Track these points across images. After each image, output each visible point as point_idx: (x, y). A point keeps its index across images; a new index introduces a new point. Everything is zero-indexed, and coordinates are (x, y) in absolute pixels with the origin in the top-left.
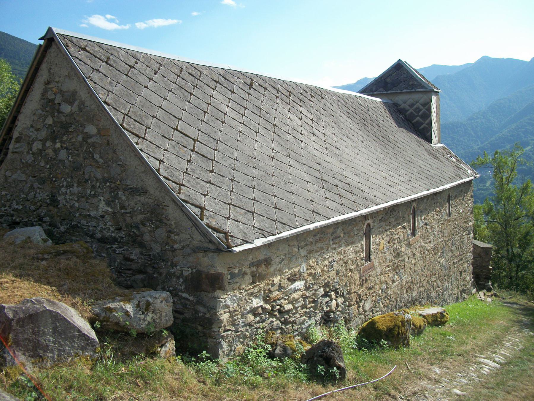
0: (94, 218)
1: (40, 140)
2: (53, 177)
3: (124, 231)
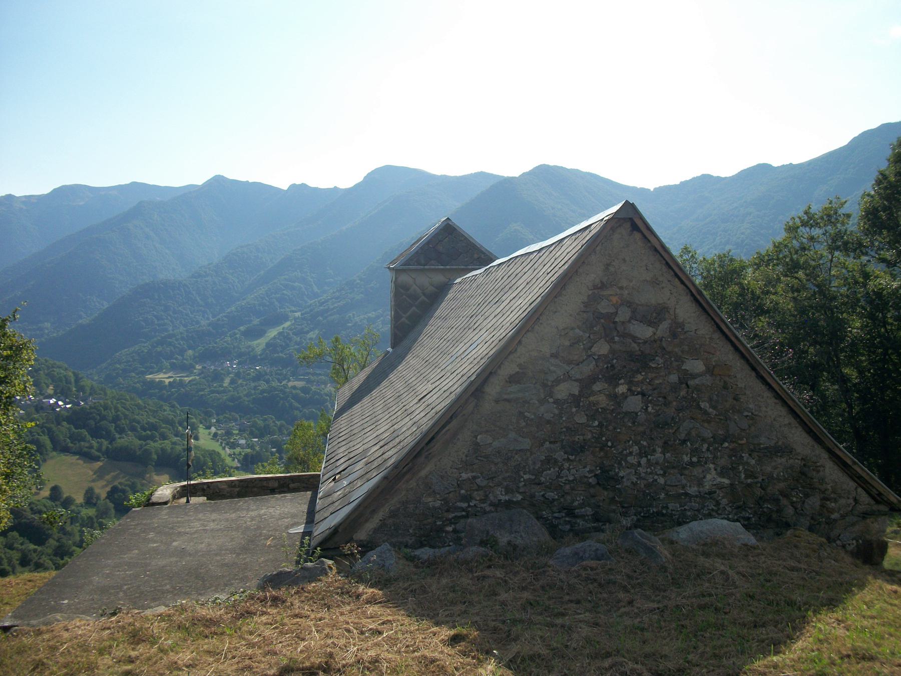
0: (696, 496)
1: (576, 380)
2: (607, 441)
3: (751, 508)
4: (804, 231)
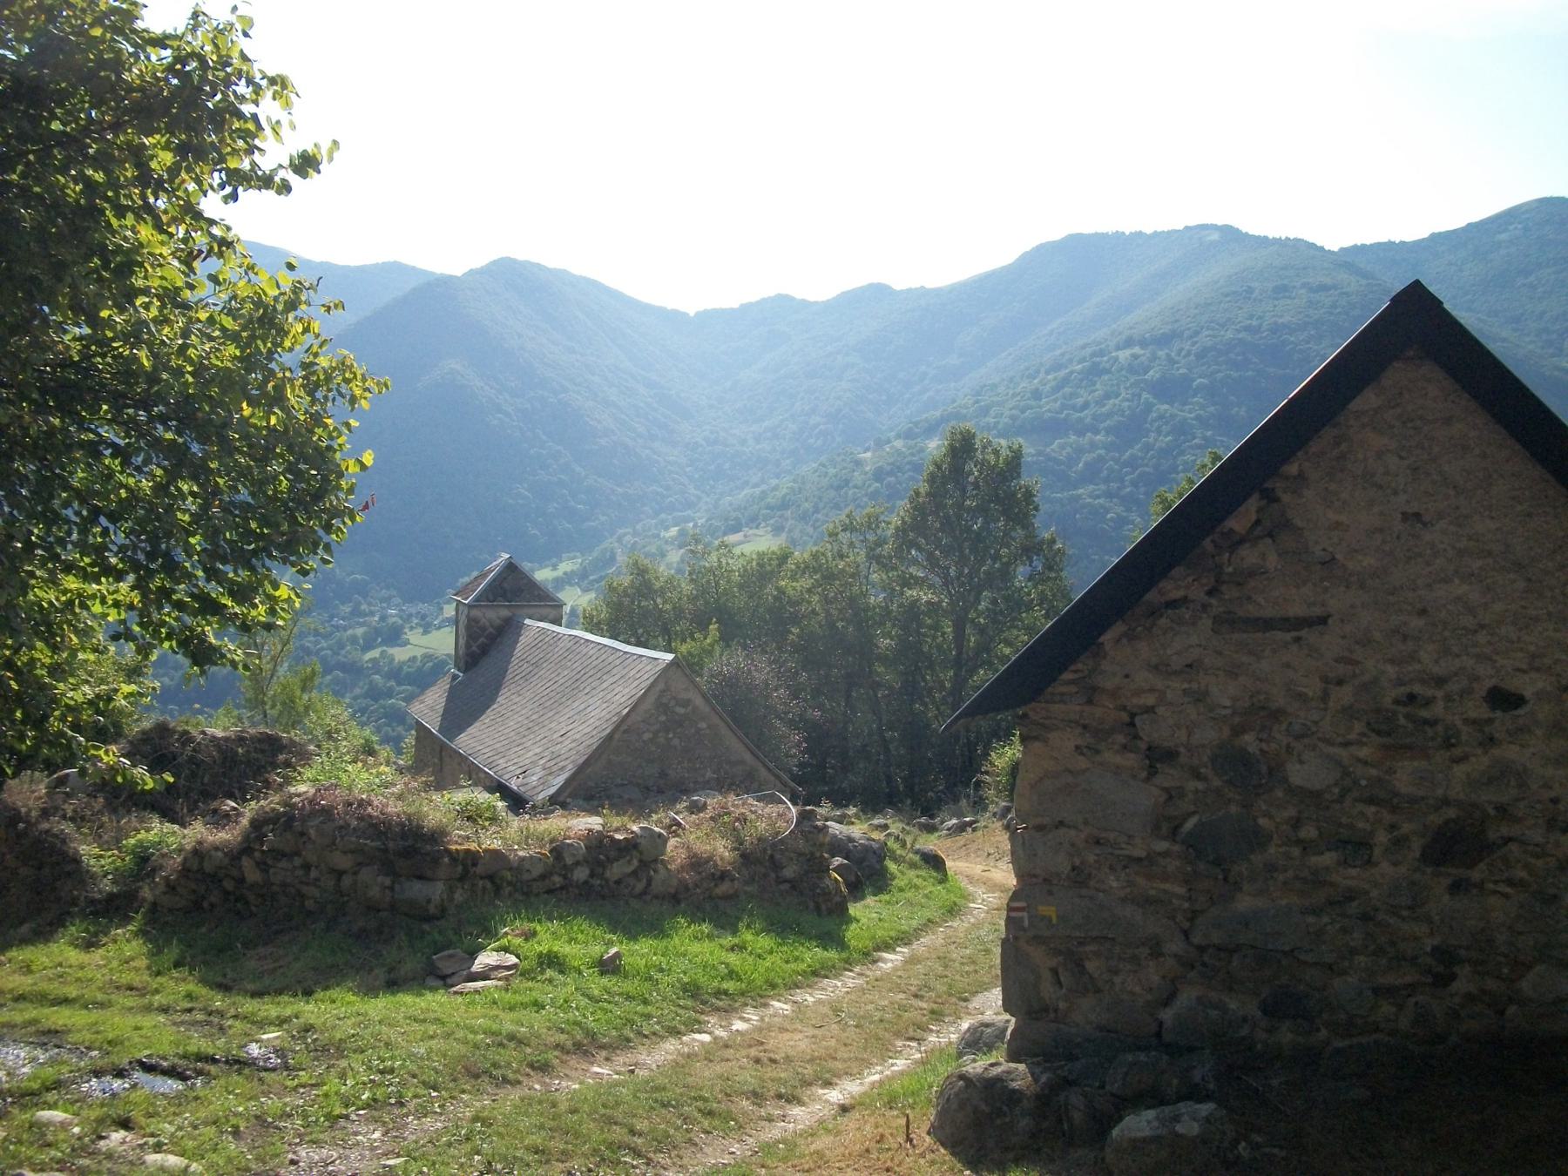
4: (844, 537)
